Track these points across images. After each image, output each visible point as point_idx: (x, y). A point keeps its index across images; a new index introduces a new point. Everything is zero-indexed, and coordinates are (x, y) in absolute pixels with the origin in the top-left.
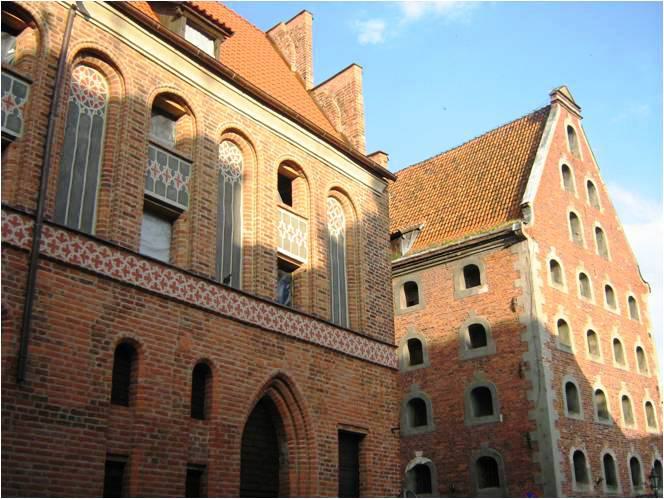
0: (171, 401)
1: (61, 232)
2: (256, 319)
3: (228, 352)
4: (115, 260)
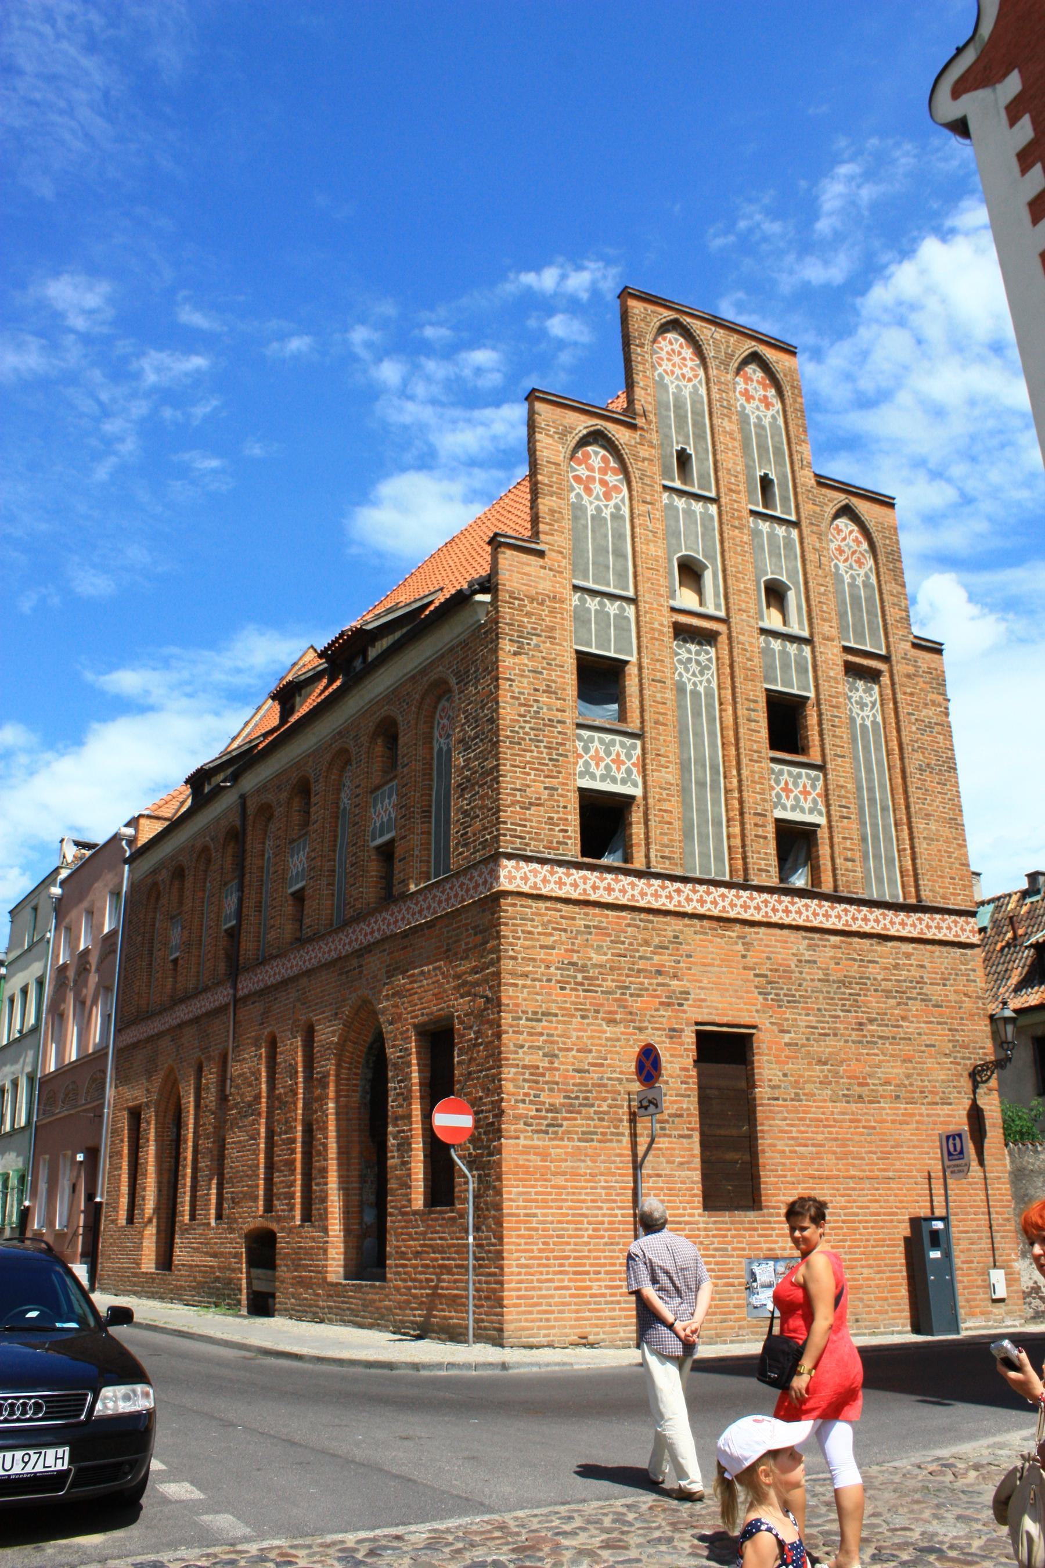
0: (399, 1036)
2: (771, 914)
3: (896, 1152)
4: (675, 891)
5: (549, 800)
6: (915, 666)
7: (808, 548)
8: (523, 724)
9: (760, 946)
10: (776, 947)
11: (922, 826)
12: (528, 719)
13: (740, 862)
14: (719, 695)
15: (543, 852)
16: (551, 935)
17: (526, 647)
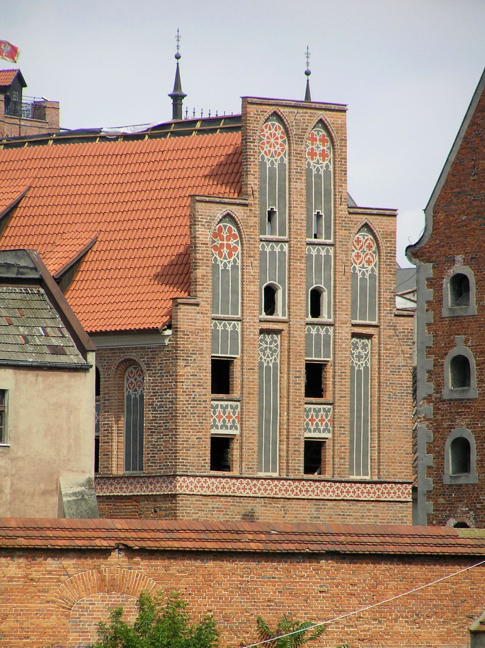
5: (198, 444)
6: (394, 329)
7: (339, 263)
8: (187, 406)
9: (292, 511)
10: (300, 510)
11: (386, 433)
12: (190, 402)
13: (285, 464)
14: (281, 367)
15: (195, 472)
16: (198, 513)
17: (190, 362)
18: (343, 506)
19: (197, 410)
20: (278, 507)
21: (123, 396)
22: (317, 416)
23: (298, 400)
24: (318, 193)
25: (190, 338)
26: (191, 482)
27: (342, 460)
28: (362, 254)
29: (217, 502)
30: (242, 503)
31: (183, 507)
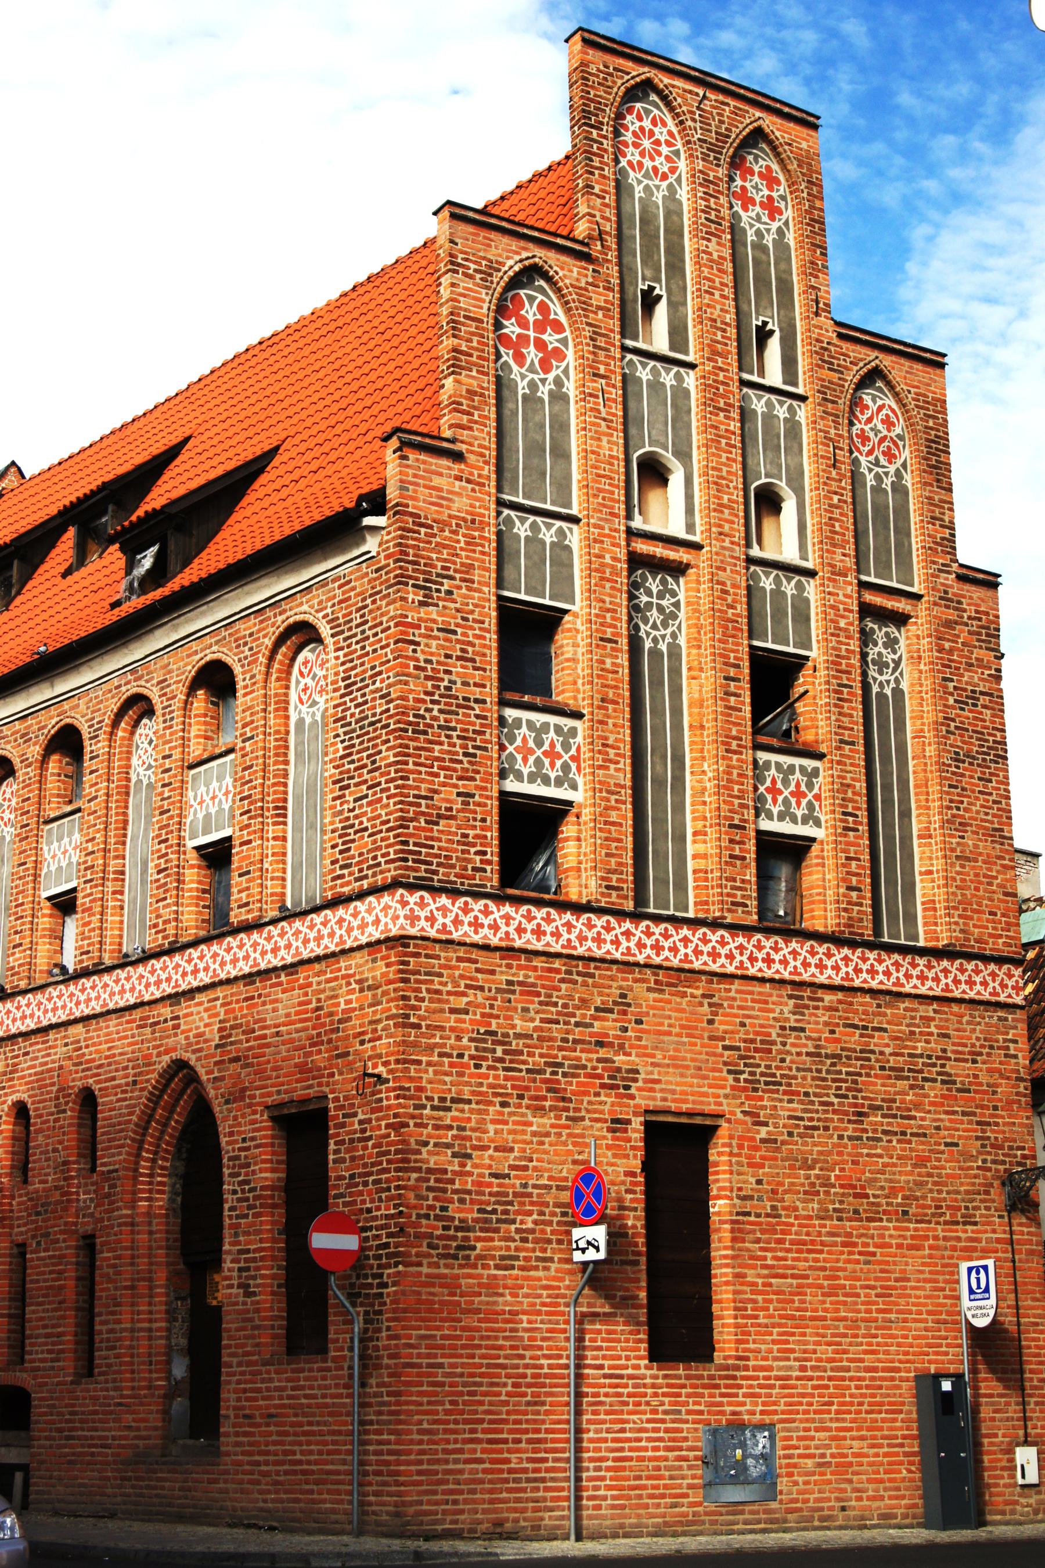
1: (483, 902)
9: (731, 1007)
16: (464, 994)
18: (861, 1004)
19: (458, 721)
20: (693, 996)
21: (287, 725)
22: (786, 782)
23: (734, 733)
24: (762, 281)
25: (434, 536)
26: (444, 910)
27: (854, 894)
28: (880, 426)
29: (520, 967)
30: (592, 976)
31: (419, 973)
